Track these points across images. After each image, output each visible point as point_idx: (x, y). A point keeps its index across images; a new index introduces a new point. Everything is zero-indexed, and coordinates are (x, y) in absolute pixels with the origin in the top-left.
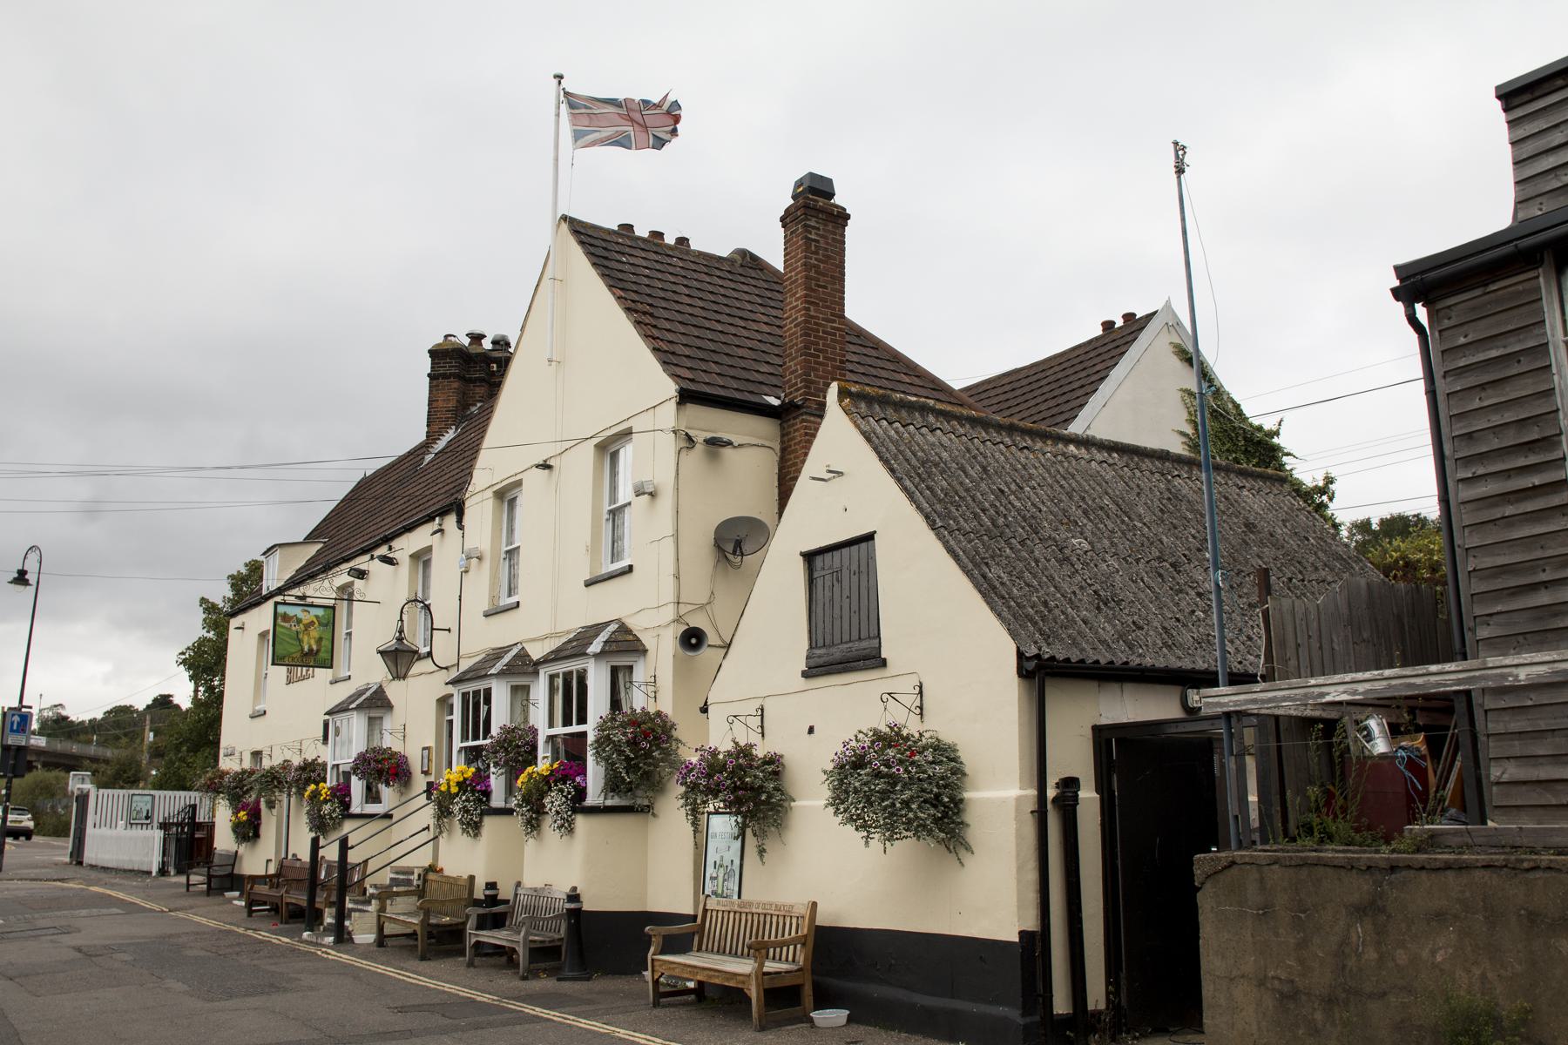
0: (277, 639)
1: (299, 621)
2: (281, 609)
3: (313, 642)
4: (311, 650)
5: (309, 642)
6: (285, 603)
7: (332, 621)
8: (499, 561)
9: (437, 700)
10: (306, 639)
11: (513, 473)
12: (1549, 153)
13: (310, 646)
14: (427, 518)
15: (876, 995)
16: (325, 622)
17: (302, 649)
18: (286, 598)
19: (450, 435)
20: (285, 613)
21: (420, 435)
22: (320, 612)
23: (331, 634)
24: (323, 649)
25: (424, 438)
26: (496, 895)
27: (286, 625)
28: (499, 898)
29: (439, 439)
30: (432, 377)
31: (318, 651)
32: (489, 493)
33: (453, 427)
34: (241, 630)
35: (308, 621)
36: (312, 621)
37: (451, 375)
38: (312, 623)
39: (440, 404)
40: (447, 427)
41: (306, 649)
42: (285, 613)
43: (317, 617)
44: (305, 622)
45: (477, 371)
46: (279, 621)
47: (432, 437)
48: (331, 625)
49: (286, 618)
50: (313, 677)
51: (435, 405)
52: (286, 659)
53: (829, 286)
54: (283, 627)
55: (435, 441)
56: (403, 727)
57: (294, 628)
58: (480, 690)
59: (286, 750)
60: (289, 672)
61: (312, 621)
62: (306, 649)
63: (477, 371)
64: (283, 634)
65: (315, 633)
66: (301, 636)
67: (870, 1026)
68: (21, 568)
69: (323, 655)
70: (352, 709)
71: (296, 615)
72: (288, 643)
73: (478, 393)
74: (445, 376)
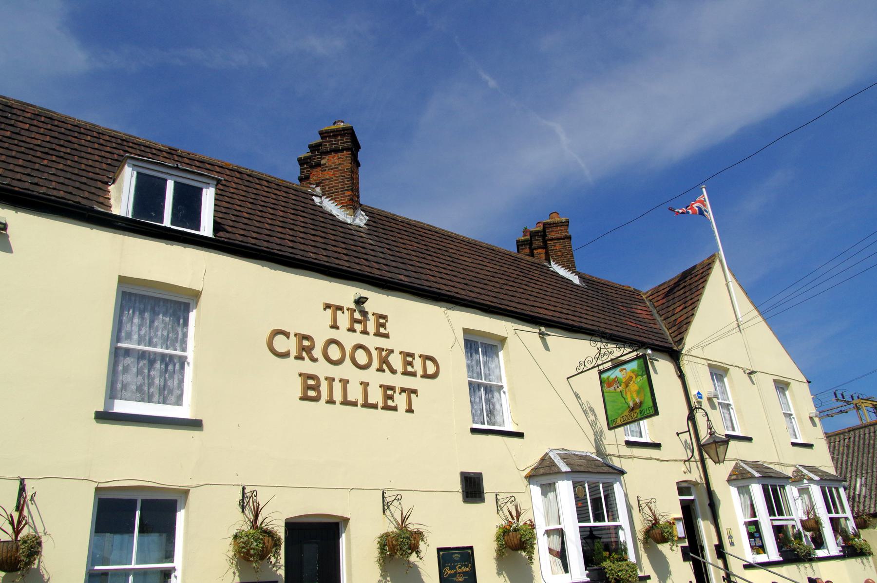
3: (635, 395)
4: (635, 404)
5: (632, 398)
17: (629, 407)
41: (631, 405)
65: (633, 387)
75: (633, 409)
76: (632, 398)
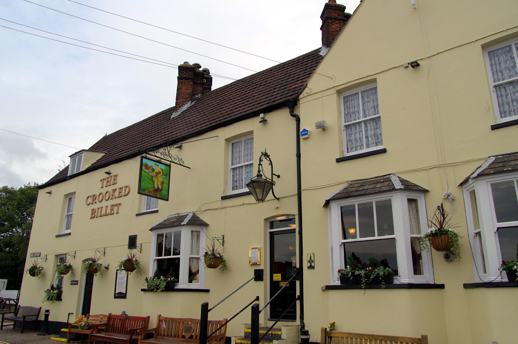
0: (142, 178)
1: (153, 170)
2: (145, 161)
4: (158, 188)
5: (157, 184)
6: (146, 158)
7: (168, 174)
8: (490, 94)
9: (264, 219)
10: (156, 181)
11: (365, 76)
12: (71, 208)
13: (158, 186)
14: (132, 156)
15: (35, 335)
16: (165, 173)
17: (154, 187)
18: (147, 155)
19: (188, 105)
21: (172, 103)
22: (163, 167)
23: (168, 181)
24: (164, 189)
25: (174, 105)
26: (308, 339)
27: (147, 171)
28: (310, 341)
29: (183, 106)
30: (179, 78)
31: (162, 189)
32: (333, 91)
33: (190, 102)
34: (49, 194)
36: (160, 172)
37: (189, 78)
38: (159, 173)
39: (183, 90)
40: (186, 102)
41: (156, 187)
42: (146, 164)
43: (162, 169)
44: (156, 171)
45: (199, 80)
46: (143, 167)
47: (179, 104)
48: (168, 176)
49: (147, 167)
50: (117, 213)
51: (180, 90)
52: (146, 191)
54: (145, 172)
55: (180, 107)
56: (74, 253)
57: (150, 174)
58: (172, 233)
59: (97, 252)
61: (160, 172)
62: (156, 187)
63: (199, 80)
65: (161, 178)
66: (154, 179)
69: (164, 192)
70: (184, 225)
73: (199, 90)
74: (186, 79)
75: (156, 190)
76: (157, 184)
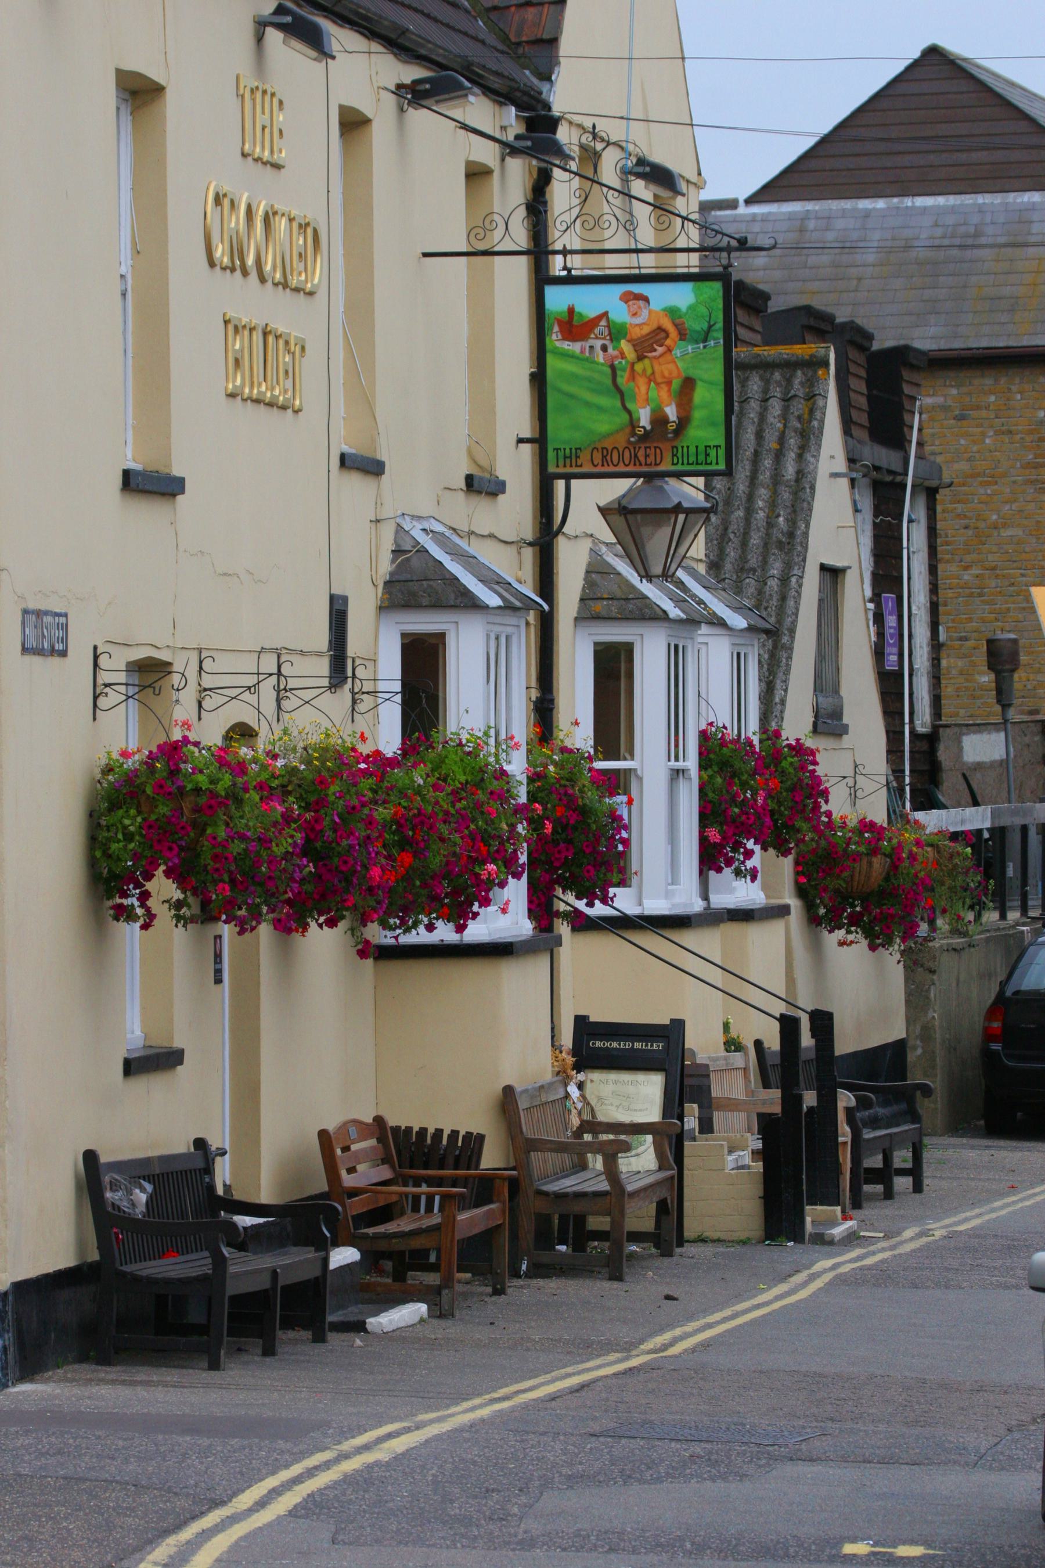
1: (616, 333)
4: (659, 420)
20: (571, 311)
24: (697, 415)
27: (575, 347)
31: (684, 422)
35: (646, 330)
36: (660, 329)
41: (644, 418)
43: (672, 312)
46: (554, 339)
53: (962, 712)
60: (926, 1135)
61: (660, 329)
64: (574, 378)
67: (47, 1370)
68: (124, 748)
71: (605, 314)
72: (588, 404)
